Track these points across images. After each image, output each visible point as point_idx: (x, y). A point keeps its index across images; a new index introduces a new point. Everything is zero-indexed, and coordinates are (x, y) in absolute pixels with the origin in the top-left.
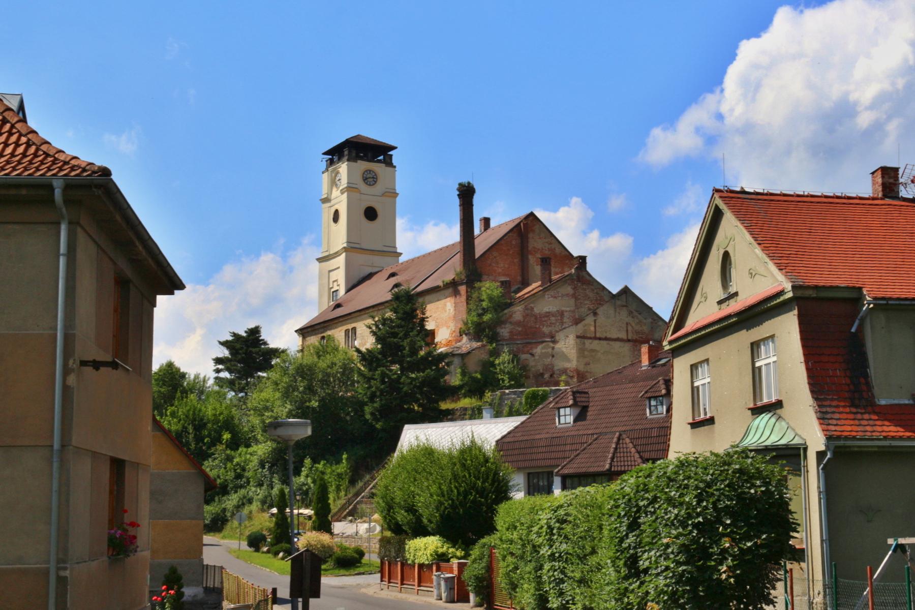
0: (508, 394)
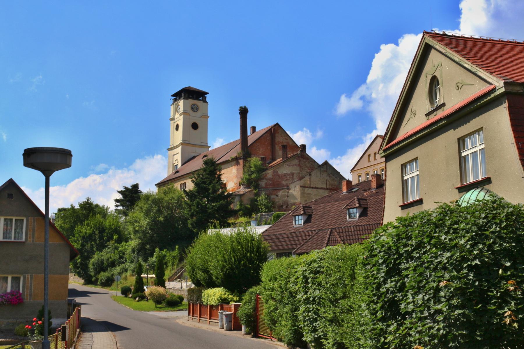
0: (264, 215)
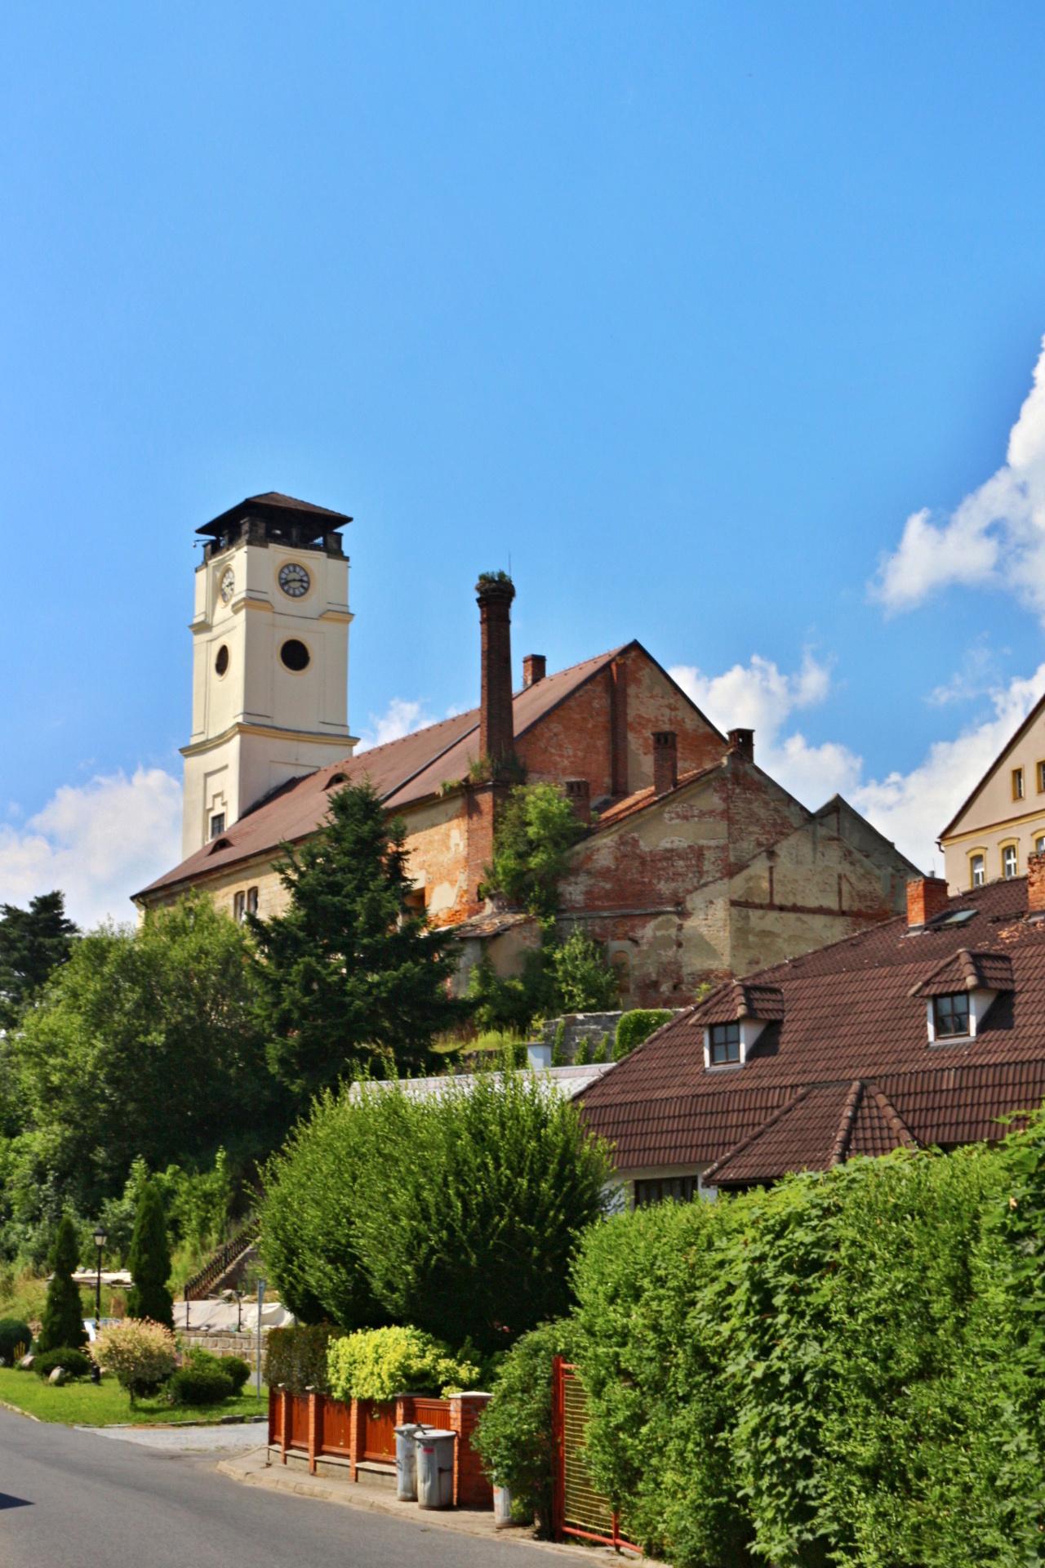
0: (582, 1023)
